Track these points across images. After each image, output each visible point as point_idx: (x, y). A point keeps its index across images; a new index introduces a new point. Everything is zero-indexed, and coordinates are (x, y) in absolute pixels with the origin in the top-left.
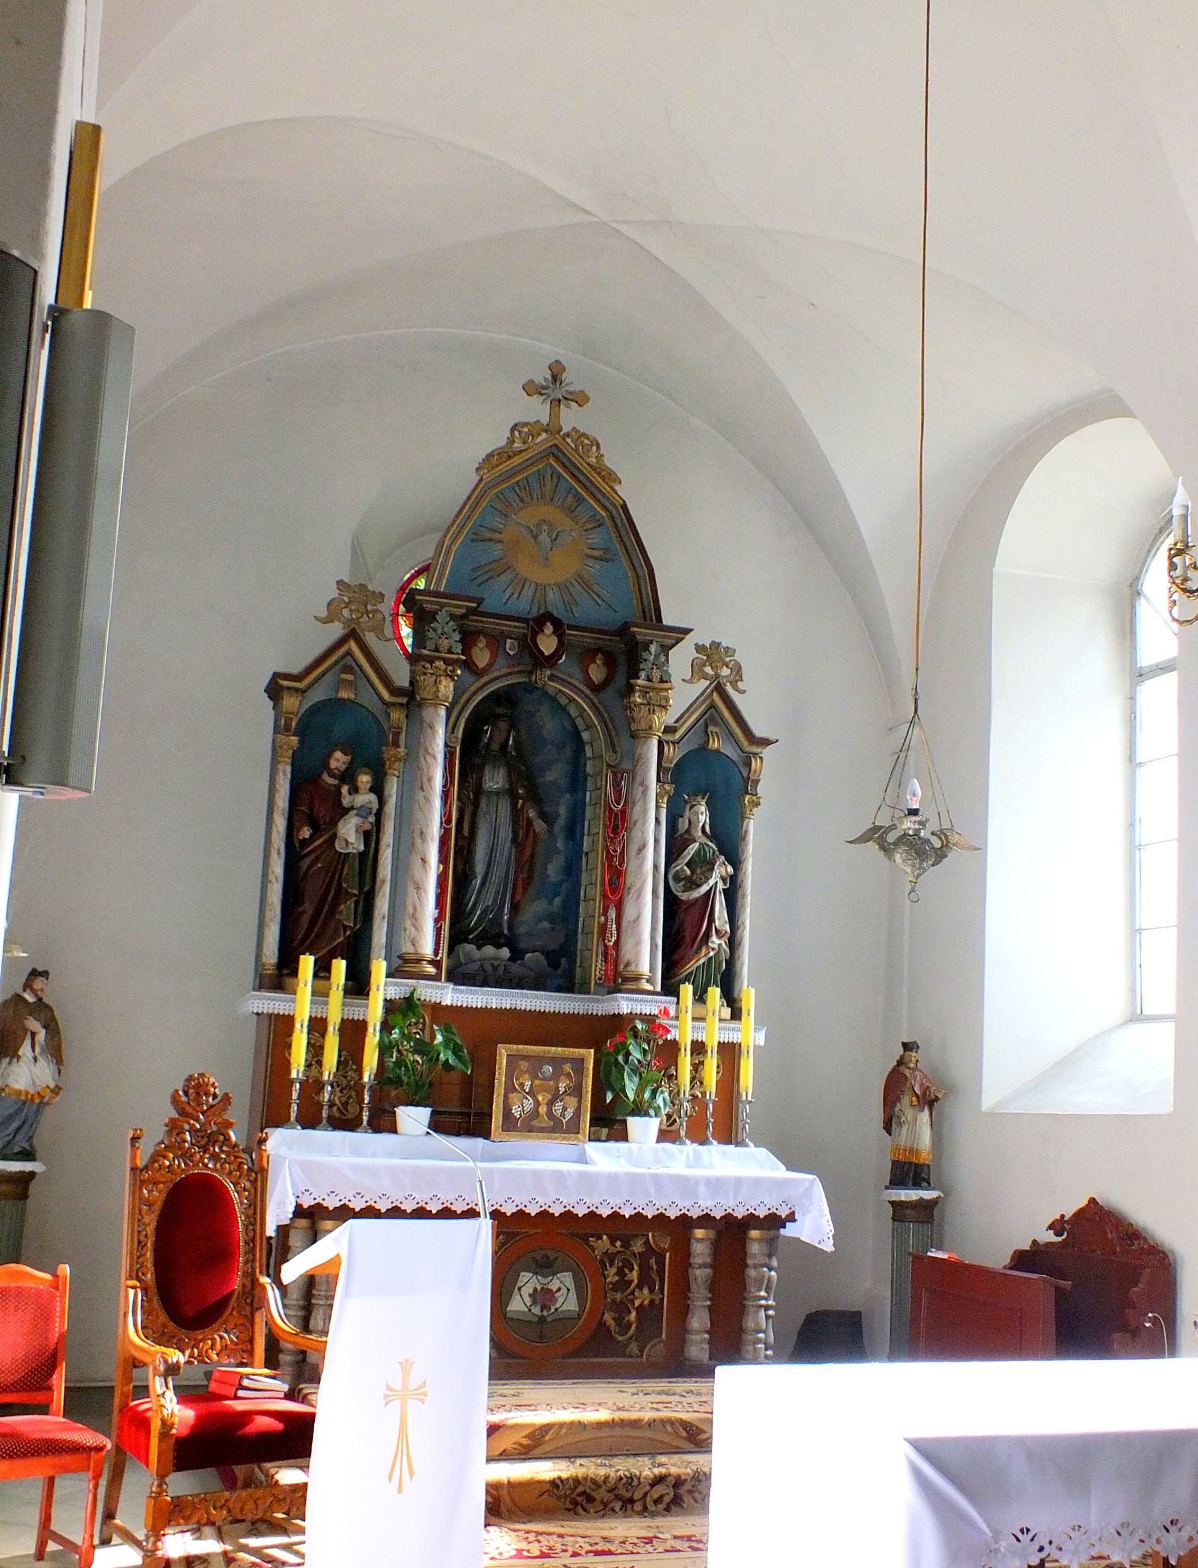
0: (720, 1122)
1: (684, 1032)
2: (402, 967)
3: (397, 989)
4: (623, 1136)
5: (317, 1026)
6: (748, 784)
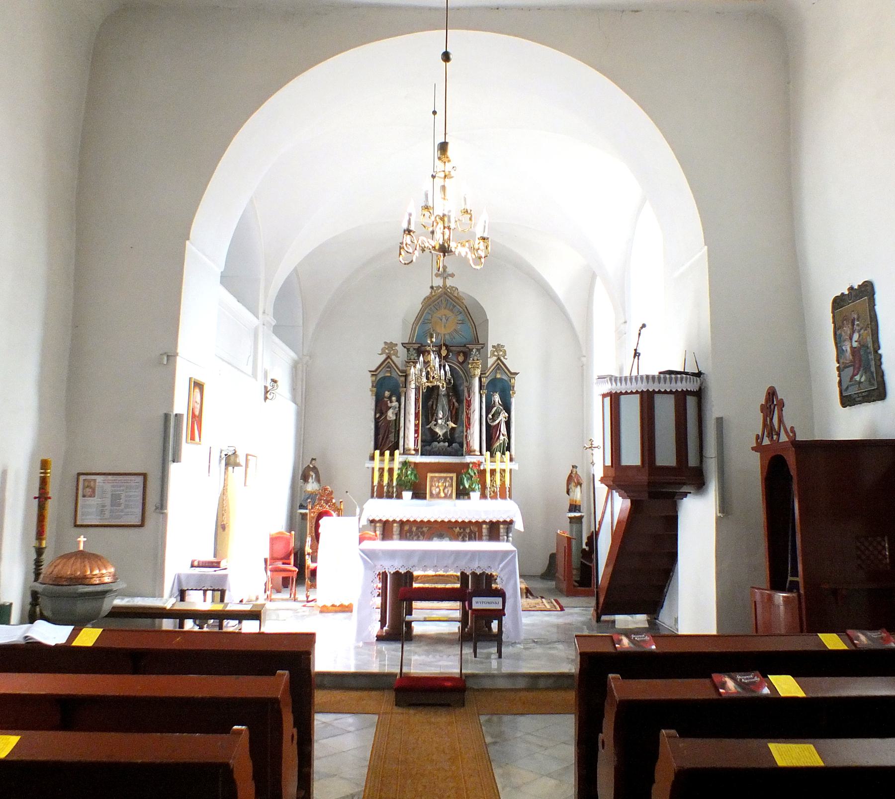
0: (503, 493)
3: (403, 458)
4: (469, 498)
5: (381, 470)
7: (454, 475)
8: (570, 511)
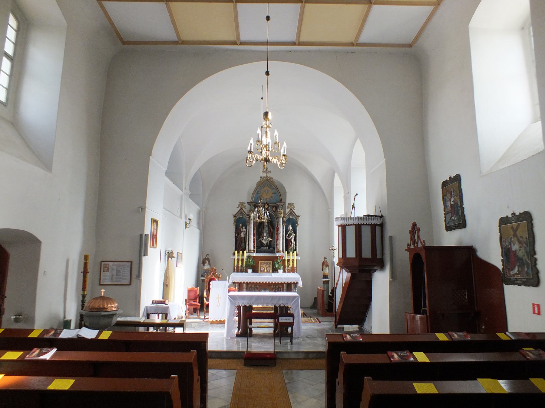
0: (293, 270)
1: (287, 258)
2: (249, 251)
3: (248, 254)
4: (278, 272)
5: (238, 260)
6: (297, 222)
7: (271, 262)
8: (324, 278)
